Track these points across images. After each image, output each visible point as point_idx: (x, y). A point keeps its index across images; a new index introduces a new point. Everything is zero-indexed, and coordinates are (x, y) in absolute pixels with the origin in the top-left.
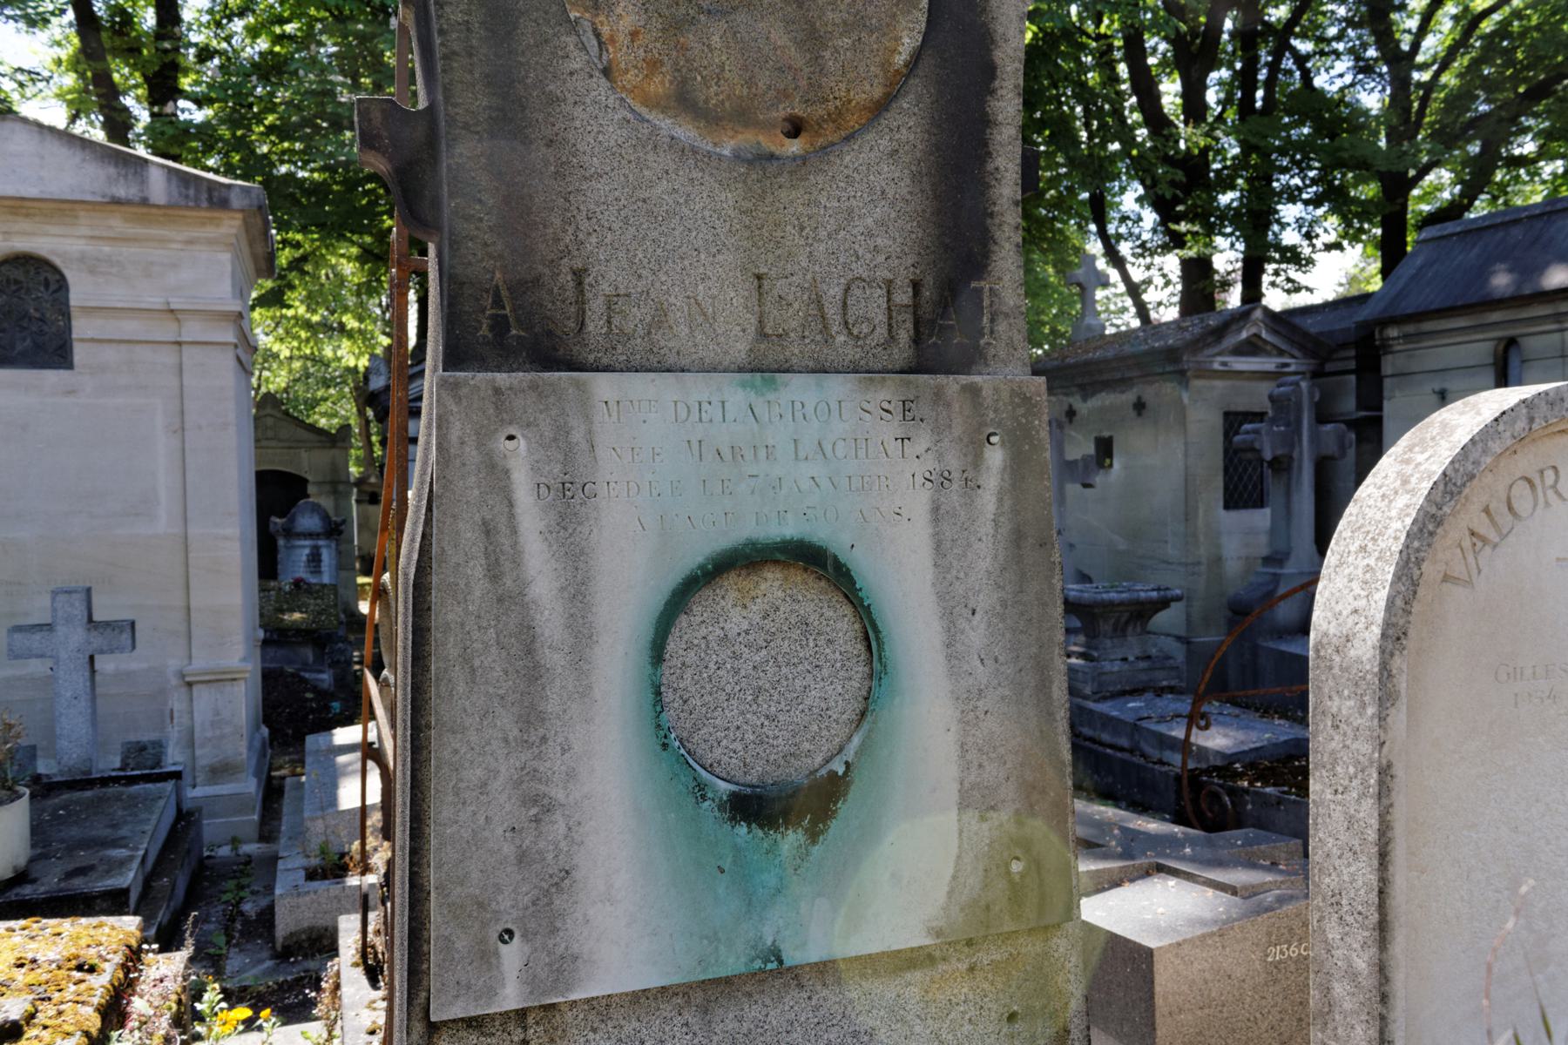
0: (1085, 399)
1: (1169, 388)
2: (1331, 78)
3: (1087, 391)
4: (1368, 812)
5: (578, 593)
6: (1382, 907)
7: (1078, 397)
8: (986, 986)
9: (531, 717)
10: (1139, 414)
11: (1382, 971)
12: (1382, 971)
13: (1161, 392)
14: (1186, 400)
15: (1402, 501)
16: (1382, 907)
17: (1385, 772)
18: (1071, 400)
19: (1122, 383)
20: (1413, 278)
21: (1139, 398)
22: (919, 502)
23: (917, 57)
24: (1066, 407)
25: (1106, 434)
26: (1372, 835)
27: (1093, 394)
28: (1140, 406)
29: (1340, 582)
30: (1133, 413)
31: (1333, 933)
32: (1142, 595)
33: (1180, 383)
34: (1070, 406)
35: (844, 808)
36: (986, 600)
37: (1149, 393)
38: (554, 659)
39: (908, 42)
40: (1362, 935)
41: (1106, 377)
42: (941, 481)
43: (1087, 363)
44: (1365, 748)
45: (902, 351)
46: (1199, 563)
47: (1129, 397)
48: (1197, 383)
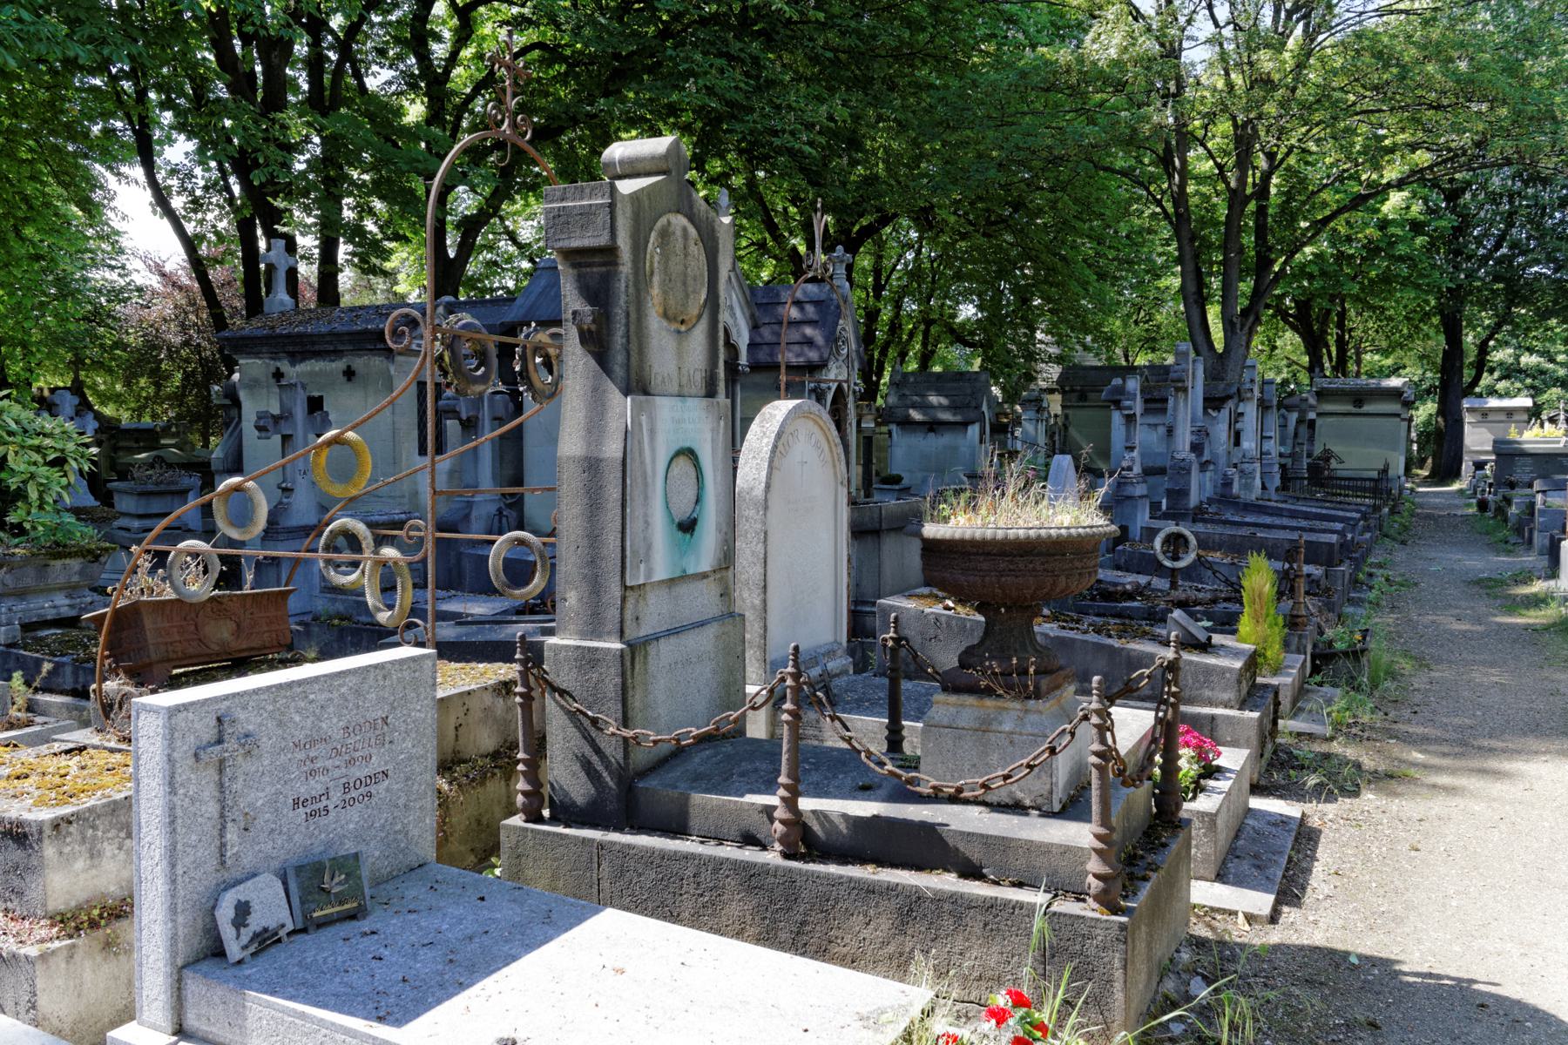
0: (293, 364)
1: (377, 362)
2: (378, 79)
3: (296, 357)
4: (760, 547)
5: (654, 461)
6: (765, 580)
7: (286, 362)
8: (1531, 108)
9: (646, 498)
10: (349, 380)
11: (765, 601)
12: (765, 601)
13: (364, 363)
14: (392, 372)
15: (765, 440)
16: (765, 580)
17: (766, 533)
18: (278, 364)
19: (336, 354)
20: (541, 294)
21: (349, 367)
22: (708, 436)
23: (706, 301)
24: (273, 370)
25: (316, 394)
26: (762, 556)
27: (303, 360)
28: (349, 374)
29: (747, 469)
30: (344, 379)
31: (746, 595)
32: (396, 517)
33: (387, 358)
34: (278, 369)
35: (697, 528)
36: (720, 467)
37: (359, 363)
38: (649, 480)
39: (703, 296)
40: (757, 592)
41: (317, 348)
42: (713, 430)
43: (300, 335)
44: (759, 526)
45: (703, 392)
46: (403, 496)
47: (340, 365)
48: (399, 359)
